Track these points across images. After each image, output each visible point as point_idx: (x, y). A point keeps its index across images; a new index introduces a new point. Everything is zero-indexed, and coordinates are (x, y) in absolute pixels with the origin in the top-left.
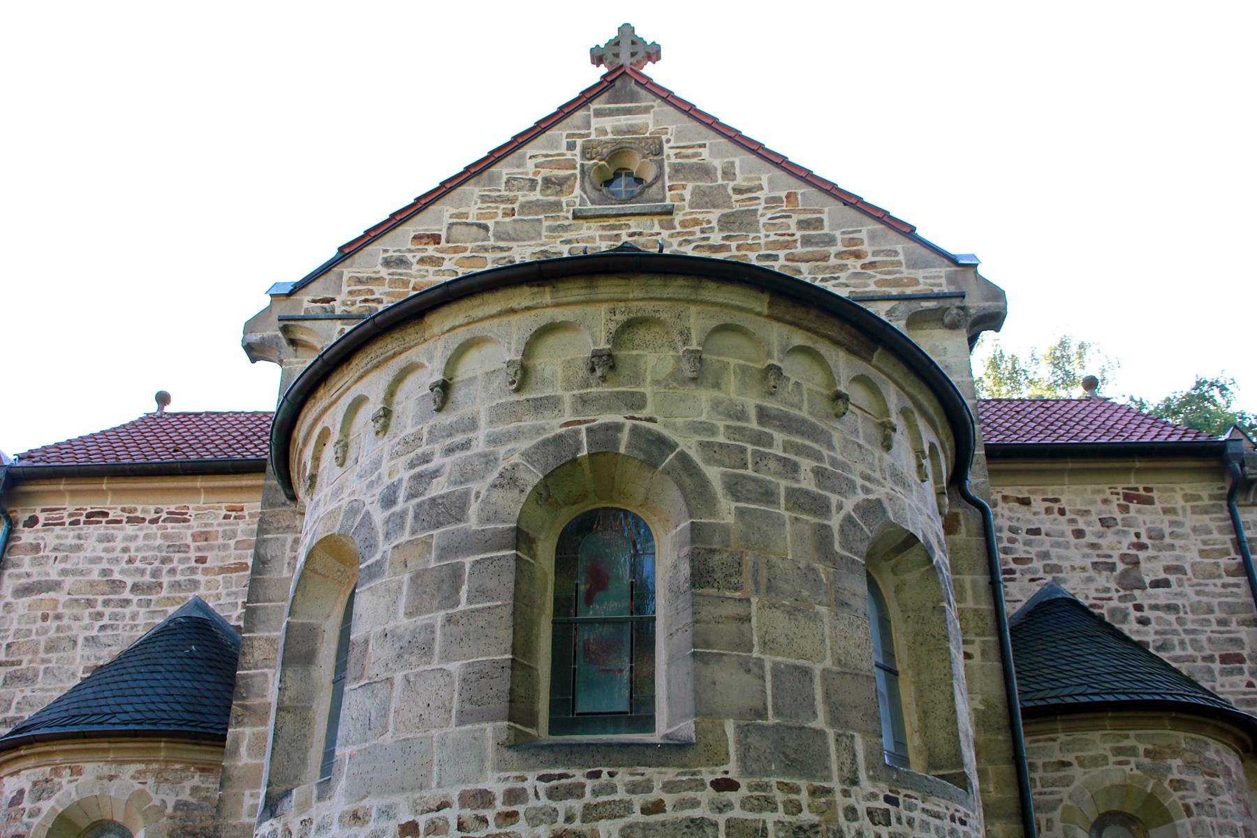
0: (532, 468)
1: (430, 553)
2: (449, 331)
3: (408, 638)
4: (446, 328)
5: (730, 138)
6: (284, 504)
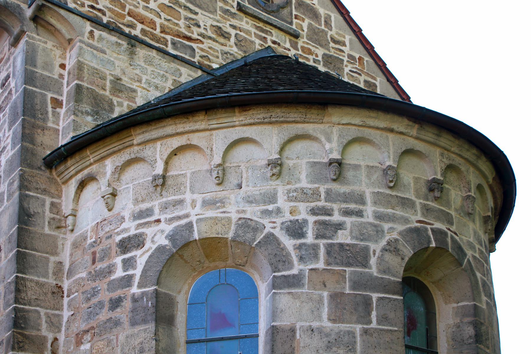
0: (406, 245)
1: (345, 283)
2: (343, 124)
3: (333, 336)
4: (344, 122)
6: (40, 168)
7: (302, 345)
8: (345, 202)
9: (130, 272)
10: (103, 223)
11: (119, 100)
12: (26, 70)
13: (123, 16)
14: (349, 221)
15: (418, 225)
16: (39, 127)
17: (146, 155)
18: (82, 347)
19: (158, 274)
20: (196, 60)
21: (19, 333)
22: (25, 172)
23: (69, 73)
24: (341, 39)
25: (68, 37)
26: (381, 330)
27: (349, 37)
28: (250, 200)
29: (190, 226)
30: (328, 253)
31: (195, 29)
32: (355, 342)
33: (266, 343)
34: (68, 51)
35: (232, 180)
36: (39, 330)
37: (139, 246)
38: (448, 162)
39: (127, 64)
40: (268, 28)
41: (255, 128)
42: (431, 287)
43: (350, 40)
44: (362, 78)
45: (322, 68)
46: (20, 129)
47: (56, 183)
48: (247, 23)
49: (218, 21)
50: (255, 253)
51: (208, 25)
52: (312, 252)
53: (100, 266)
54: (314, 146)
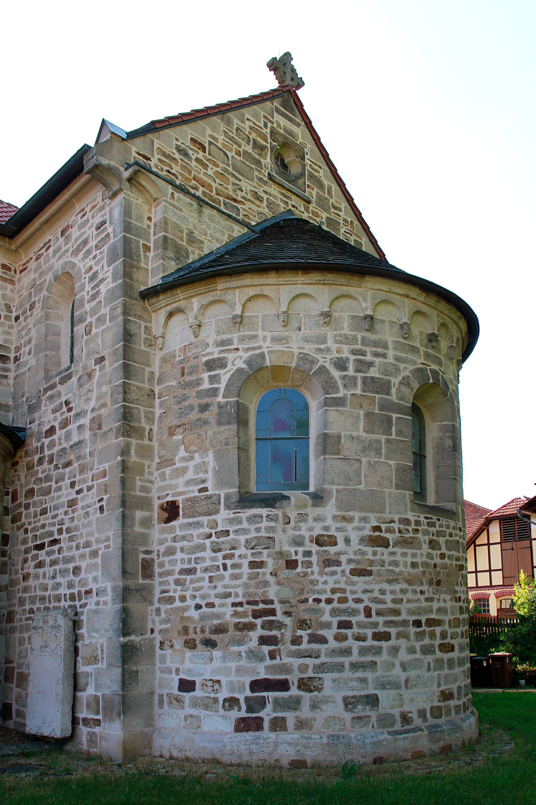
5: (331, 170)
6: (136, 299)
7: (345, 447)
8: (375, 347)
9: (216, 386)
10: (190, 346)
11: (192, 249)
12: (125, 220)
13: (190, 180)
14: (378, 360)
15: (422, 366)
16: (135, 267)
17: (227, 299)
18: (175, 438)
19: (238, 389)
20: (240, 218)
21: (127, 424)
22: (127, 302)
23: (155, 226)
24: (339, 206)
25: (155, 196)
26: (399, 440)
27: (344, 205)
28: (307, 340)
29: (262, 355)
30: (364, 383)
31: (239, 192)
32: (381, 448)
33: (317, 444)
34: (153, 206)
35: (294, 324)
36: (140, 422)
37: (222, 366)
38: (441, 321)
39: (197, 221)
40: (289, 194)
41: (312, 286)
42: (423, 409)
43: (345, 207)
44: (353, 238)
45: (324, 227)
46: (121, 268)
47: (148, 311)
48: (275, 190)
49: (255, 187)
50: (310, 380)
51: (248, 190)
52: (352, 381)
53: (188, 378)
54: (354, 303)
